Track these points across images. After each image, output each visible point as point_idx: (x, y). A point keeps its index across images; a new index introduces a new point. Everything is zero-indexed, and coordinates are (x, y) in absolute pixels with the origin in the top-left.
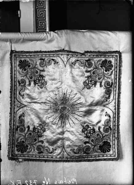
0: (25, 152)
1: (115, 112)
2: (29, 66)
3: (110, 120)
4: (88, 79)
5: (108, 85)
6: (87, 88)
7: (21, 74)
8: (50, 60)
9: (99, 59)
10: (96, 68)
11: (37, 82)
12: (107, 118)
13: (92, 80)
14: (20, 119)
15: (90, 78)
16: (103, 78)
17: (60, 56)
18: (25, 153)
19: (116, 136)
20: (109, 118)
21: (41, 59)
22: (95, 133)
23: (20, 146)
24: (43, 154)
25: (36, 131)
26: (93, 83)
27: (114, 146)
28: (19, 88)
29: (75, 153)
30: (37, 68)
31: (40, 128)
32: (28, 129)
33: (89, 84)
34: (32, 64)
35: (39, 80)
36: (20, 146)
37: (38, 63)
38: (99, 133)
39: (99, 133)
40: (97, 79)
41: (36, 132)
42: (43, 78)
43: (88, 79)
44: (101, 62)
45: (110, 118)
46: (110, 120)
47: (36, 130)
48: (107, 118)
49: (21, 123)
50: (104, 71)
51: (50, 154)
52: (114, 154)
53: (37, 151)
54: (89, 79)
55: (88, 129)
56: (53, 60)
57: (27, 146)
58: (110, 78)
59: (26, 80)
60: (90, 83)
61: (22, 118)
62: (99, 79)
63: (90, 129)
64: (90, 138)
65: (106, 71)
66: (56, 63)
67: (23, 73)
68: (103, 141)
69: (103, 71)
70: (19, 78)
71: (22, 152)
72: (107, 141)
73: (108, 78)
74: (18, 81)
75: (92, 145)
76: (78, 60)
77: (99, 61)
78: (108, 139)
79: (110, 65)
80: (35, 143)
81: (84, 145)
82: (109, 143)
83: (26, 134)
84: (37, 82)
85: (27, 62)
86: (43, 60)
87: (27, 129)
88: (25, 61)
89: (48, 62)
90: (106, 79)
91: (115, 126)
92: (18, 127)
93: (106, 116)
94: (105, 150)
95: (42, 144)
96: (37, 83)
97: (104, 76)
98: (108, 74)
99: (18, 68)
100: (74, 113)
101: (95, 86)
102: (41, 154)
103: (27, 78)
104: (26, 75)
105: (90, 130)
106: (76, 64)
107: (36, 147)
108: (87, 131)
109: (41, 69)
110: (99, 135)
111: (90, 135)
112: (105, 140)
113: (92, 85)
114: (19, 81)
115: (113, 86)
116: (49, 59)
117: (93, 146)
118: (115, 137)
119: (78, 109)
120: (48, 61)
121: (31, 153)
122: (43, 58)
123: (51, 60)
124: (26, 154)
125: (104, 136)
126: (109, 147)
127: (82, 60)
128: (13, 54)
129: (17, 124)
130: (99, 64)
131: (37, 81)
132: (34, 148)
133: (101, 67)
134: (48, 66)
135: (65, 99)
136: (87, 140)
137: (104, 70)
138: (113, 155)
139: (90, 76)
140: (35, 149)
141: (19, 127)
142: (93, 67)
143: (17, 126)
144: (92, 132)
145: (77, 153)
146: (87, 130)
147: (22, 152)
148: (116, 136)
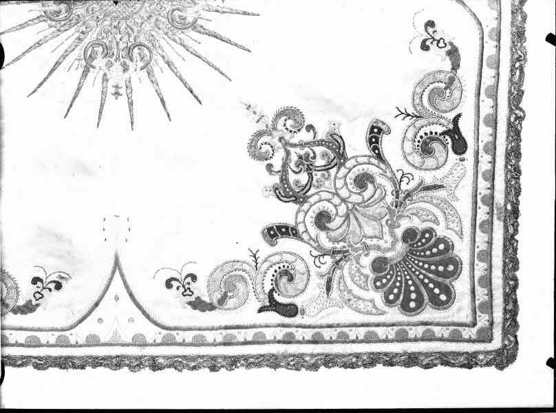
1: (494, 24)
2: (379, 265)
11: (324, 155)
12: (437, 60)
19: (500, 197)
20: (447, 65)
21: (290, 310)
22: (340, 165)
27: (480, 268)
29: (198, 305)
38: (373, 170)
45: (455, 66)
46: (452, 80)
52: (483, 320)
55: (295, 140)
64: (305, 199)
68: (405, 224)
74: (469, 154)
78: (441, 218)
81: (265, 249)
82: (449, 247)
84: (324, 155)
85: (397, 296)
86: (273, 306)
88: (405, 308)
89: (240, 286)
91: (493, 122)
93: (425, 47)
94: (418, 291)
99: (462, 250)
100: (193, 26)
105: (307, 144)
108: (288, 153)
112: (418, 224)
118: (489, 202)
122: (273, 317)
123: (215, 302)
125: (409, 195)
126: (446, 275)
128: (496, 343)
131: (320, 162)
136: (286, 213)
145: (211, 307)
148: (500, 197)
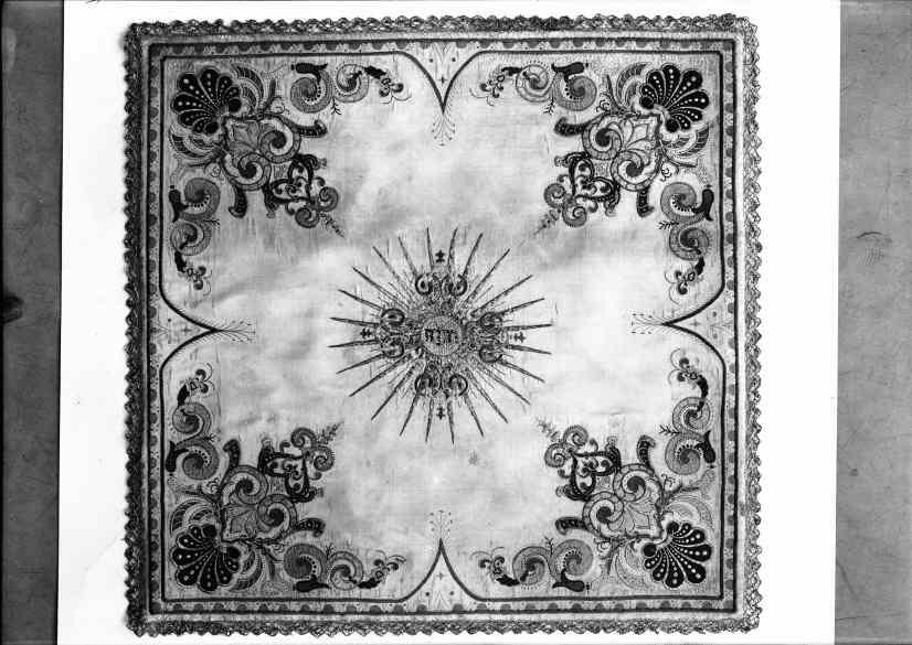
0: (236, 570)
2: (236, 106)
3: (702, 404)
4: (572, 171)
5: (682, 208)
6: (567, 222)
7: (194, 155)
8: (356, 75)
9: (632, 60)
10: (618, 111)
11: (280, 192)
13: (592, 178)
14: (188, 408)
15: (587, 165)
16: (653, 164)
17: (413, 49)
18: (223, 591)
20: (698, 392)
23: (192, 553)
24: (326, 593)
25: (278, 470)
26: (599, 193)
28: (170, 227)
30: (278, 116)
31: (580, 201)
32: (645, 199)
33: (580, 201)
34: (250, 95)
35: (590, 470)
36: (192, 553)
37: (283, 90)
39: (242, 180)
40: (622, 169)
41: (279, 475)
42: (317, 173)
43: (572, 171)
44: (641, 80)
45: (705, 393)
47: (275, 465)
48: (690, 390)
49: (689, 236)
50: (663, 130)
51: (365, 593)
53: (287, 577)
54: (577, 172)
56: (375, 73)
57: (235, 553)
58: (689, 166)
59: (218, 182)
60: (293, 463)
61: (684, 266)
62: (634, 170)
63: (291, 205)
65: (672, 127)
66: (391, 87)
67: (200, 143)
69: (657, 128)
70: (175, 171)
71: (208, 585)
72: (195, 130)
73: (682, 164)
75: (278, 116)
76: (512, 70)
77: (637, 69)
79: (692, 96)
80: (280, 537)
83: (224, 485)
84: (280, 192)
87: (224, 459)
88: (669, 583)
89: (345, 84)
90: (673, 169)
92: (175, 451)
95: (562, 120)
96: (286, 202)
97: (662, 154)
98: (682, 142)
99: (171, 118)
101: (610, 208)
102: (314, 594)
103: (222, 175)
104: (219, 158)
106: (502, 88)
107: (281, 556)
109: (305, 120)
110: (644, 485)
111: (588, 481)
113: (286, 450)
114: (174, 195)
115: (714, 212)
116: (350, 70)
117: (274, 108)
119: (522, 338)
120: (342, 77)
121: (251, 592)
124: (231, 595)
125: (672, 494)
127: (537, 70)
129: (172, 435)
130: (634, 86)
132: (272, 560)
133: (646, 103)
134: (341, 106)
135: (437, 383)
137: (660, 122)
138: (721, 605)
139: (585, 155)
140: (277, 565)
141: (184, 450)
142: (596, 104)
143: (710, 219)
144: (601, 469)
146: (309, 199)
147: (208, 585)
